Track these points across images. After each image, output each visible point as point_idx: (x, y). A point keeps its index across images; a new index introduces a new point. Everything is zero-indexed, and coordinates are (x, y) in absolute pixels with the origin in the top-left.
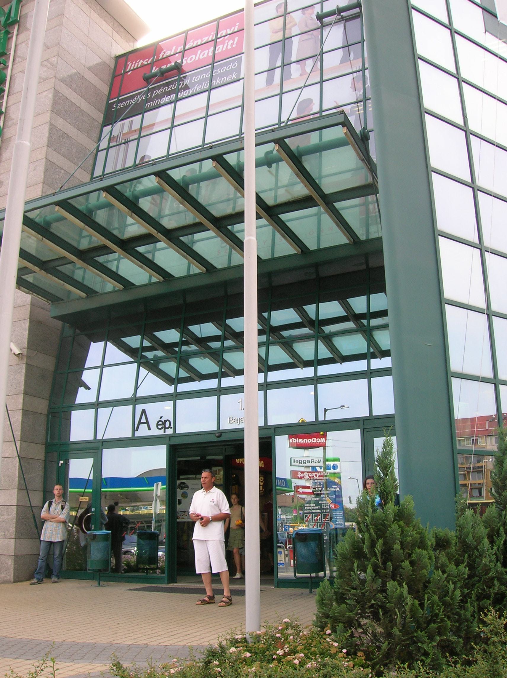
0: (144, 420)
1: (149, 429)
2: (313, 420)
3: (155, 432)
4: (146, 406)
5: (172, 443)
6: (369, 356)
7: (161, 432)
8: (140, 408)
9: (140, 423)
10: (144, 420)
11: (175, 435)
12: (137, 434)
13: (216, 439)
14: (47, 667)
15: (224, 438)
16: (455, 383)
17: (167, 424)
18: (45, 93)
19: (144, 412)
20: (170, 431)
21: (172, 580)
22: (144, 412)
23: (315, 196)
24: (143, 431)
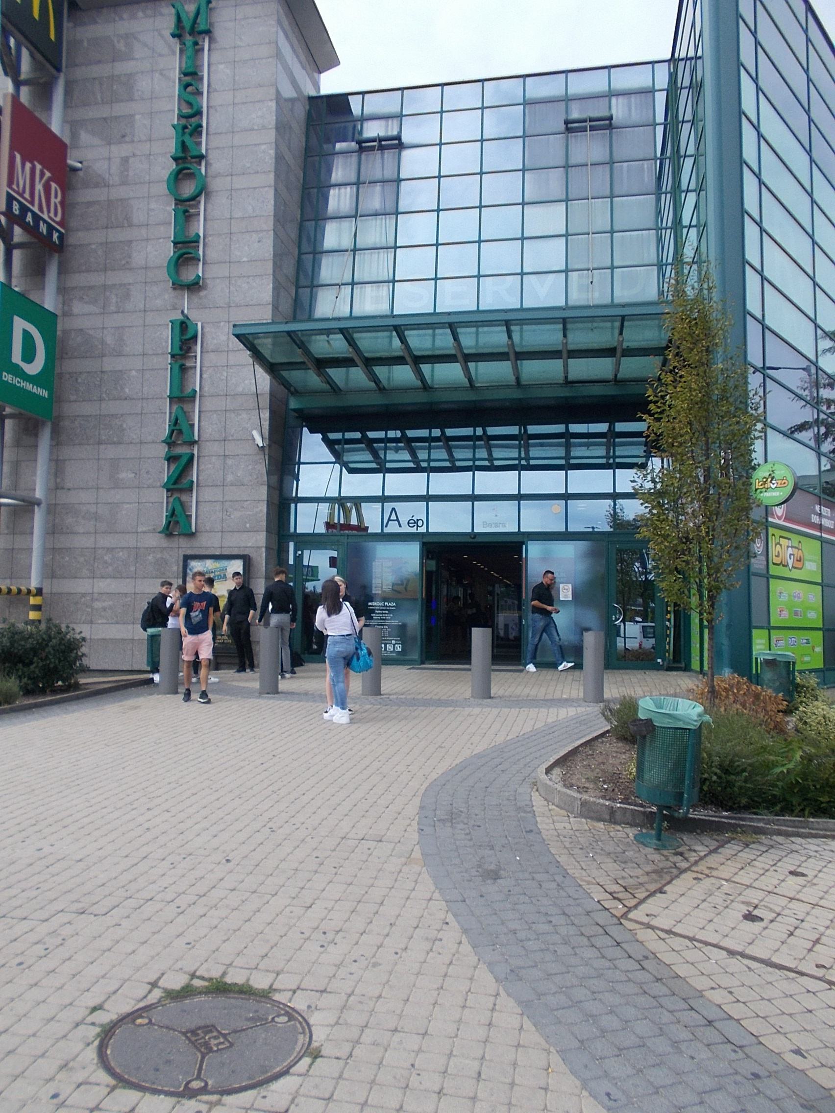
0: (393, 517)
1: (400, 526)
2: (517, 530)
3: (406, 529)
4: (398, 505)
5: (425, 540)
6: (429, 470)
7: (414, 530)
8: (389, 506)
9: (389, 520)
10: (393, 517)
11: (428, 534)
12: (386, 530)
13: (470, 540)
14: (638, 877)
15: (479, 539)
16: (752, 577)
17: (420, 523)
18: (263, 147)
19: (393, 509)
20: (423, 530)
21: (423, 663)
22: (393, 509)
23: (356, 358)
24: (393, 528)
